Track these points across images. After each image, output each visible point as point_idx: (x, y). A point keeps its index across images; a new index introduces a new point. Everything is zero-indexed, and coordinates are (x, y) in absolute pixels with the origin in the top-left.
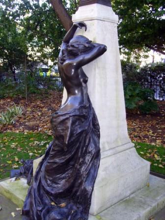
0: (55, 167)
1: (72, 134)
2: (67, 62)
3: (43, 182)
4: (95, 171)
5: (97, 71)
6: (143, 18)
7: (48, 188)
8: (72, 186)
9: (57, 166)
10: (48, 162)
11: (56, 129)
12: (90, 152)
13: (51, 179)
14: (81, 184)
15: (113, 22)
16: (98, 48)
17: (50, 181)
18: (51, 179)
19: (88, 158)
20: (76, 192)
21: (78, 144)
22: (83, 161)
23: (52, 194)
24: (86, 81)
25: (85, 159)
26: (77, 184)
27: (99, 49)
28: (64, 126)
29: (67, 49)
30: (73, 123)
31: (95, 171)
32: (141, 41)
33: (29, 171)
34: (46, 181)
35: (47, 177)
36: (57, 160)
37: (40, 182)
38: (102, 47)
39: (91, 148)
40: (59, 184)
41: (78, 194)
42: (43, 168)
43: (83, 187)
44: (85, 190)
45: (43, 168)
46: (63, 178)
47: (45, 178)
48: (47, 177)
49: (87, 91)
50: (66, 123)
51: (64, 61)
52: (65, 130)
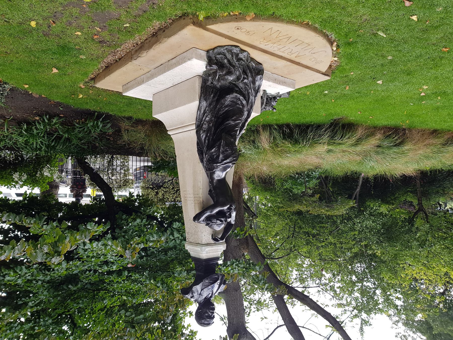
0: (234, 116)
2: (225, 208)
3: (244, 102)
5: (201, 196)
7: (241, 98)
8: (218, 101)
9: (232, 117)
10: (240, 120)
11: (232, 151)
12: (204, 131)
14: (210, 105)
15: (191, 243)
16: (201, 220)
17: (238, 104)
19: (205, 126)
20: (214, 97)
22: (210, 123)
23: (236, 92)
24: (210, 191)
25: (208, 125)
26: (214, 104)
27: (199, 220)
29: (226, 218)
30: (218, 157)
33: (34, 324)
34: (242, 103)
35: (241, 107)
37: (248, 102)
39: (203, 136)
41: (212, 96)
42: (246, 113)
43: (208, 102)
44: (206, 100)
45: (246, 113)
46: (227, 106)
47: (243, 106)
48: (241, 107)
49: (203, 165)
51: (228, 208)
52: (224, 151)
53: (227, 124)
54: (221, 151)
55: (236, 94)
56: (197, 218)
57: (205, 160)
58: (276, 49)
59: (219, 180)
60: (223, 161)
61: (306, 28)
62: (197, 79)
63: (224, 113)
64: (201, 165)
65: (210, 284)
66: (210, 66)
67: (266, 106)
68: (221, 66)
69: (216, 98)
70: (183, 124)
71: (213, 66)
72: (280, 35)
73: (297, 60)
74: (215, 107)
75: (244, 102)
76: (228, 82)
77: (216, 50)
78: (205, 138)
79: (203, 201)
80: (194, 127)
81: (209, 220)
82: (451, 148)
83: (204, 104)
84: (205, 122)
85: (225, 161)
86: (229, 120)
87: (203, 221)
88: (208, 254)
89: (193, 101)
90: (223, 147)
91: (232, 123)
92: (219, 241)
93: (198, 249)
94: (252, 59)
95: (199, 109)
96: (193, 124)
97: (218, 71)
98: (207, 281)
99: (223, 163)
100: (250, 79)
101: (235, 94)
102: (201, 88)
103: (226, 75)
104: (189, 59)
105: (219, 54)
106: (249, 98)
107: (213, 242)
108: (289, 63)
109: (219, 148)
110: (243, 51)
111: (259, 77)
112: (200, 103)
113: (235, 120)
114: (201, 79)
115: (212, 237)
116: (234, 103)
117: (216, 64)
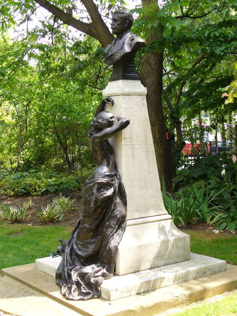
3: (75, 247)
7: (78, 252)
20: (103, 253)
34: (77, 245)
35: (78, 242)
37: (72, 247)
43: (108, 248)
46: (93, 243)
48: (78, 242)
49: (120, 179)
61: (115, 263)
65: (115, 54)
74: (102, 241)
80: (128, 223)
82: (236, 291)
84: (113, 226)
85: (91, 184)
93: (127, 90)
98: (117, 57)
114: (117, 272)
116: (85, 246)
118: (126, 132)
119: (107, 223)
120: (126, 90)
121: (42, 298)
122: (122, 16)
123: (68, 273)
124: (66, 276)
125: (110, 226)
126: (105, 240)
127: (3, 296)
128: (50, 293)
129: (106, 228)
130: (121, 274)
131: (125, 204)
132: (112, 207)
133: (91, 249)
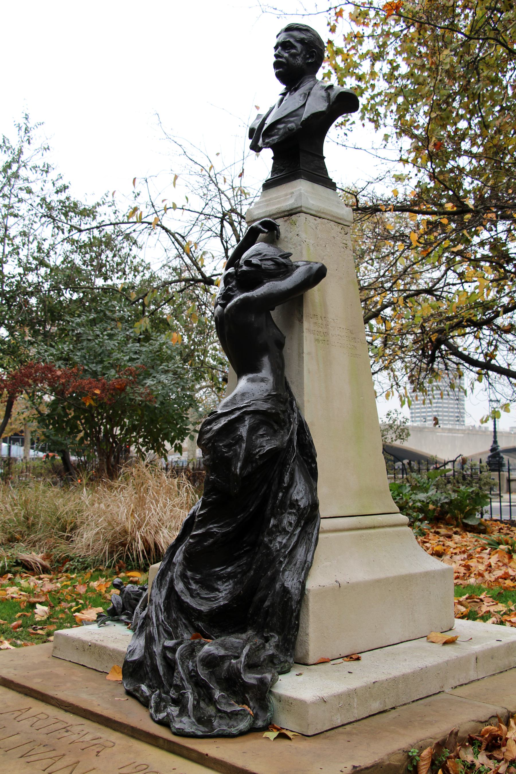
1: (249, 457)
3: (179, 586)
4: (307, 551)
6: (96, 453)
7: (187, 599)
9: (214, 543)
13: (198, 577)
14: (274, 579)
17: (196, 582)
18: (198, 577)
20: (263, 600)
21: (265, 488)
25: (281, 521)
26: (263, 582)
28: (232, 436)
30: (252, 430)
31: (307, 551)
32: (24, 365)
34: (187, 584)
36: (214, 528)
37: (171, 589)
38: (316, 267)
39: (299, 493)
40: (218, 590)
41: (267, 603)
43: (278, 586)
44: (285, 590)
47: (183, 577)
48: (189, 573)
49: (299, 416)
50: (237, 429)
52: (234, 445)
53: (228, 525)
54: (244, 445)
55: (202, 608)
56: (318, 275)
57: (295, 426)
58: (76, 729)
59: (256, 369)
60: (240, 420)
62: (311, 654)
63: (239, 558)
64: (308, 418)
66: (262, 681)
67: (140, 595)
68: (233, 685)
69: (256, 598)
70: (361, 536)
71: (253, 682)
72: (50, 761)
73: (29, 702)
75: (179, 586)
76: (219, 640)
77: (243, 725)
78: (291, 485)
79: (301, 320)
80: (324, 524)
81: (283, 268)
83: (290, 580)
84: (290, 529)
85: (233, 417)
86: (224, 535)
87: (298, 267)
88: (290, 191)
89: (324, 592)
90: (236, 455)
91: (214, 528)
92: (261, 224)
94: (145, 703)
95: (306, 568)
96: (325, 532)
97: (241, 666)
99: (237, 414)
100: (157, 649)
101: (204, 608)
102: (298, 625)
103: (223, 658)
104: (324, 701)
105: (233, 715)
106: (167, 597)
107: (279, 222)
108: (51, 693)
109: (248, 451)
110: (165, 723)
111: (136, 657)
112: (303, 584)
113: (208, 534)
114: (299, 653)
115: (278, 232)
117: (246, 687)
118: (314, 293)
119: (272, 522)
120: (311, 202)
121: (311, 613)
122: (303, 36)
123: (165, 658)
124: (161, 669)
125: (280, 530)
126: (269, 565)
127: (513, 643)
128: (183, 547)
129: (271, 533)
130: (311, 661)
131: (312, 474)
132: (286, 479)
133: (223, 593)
